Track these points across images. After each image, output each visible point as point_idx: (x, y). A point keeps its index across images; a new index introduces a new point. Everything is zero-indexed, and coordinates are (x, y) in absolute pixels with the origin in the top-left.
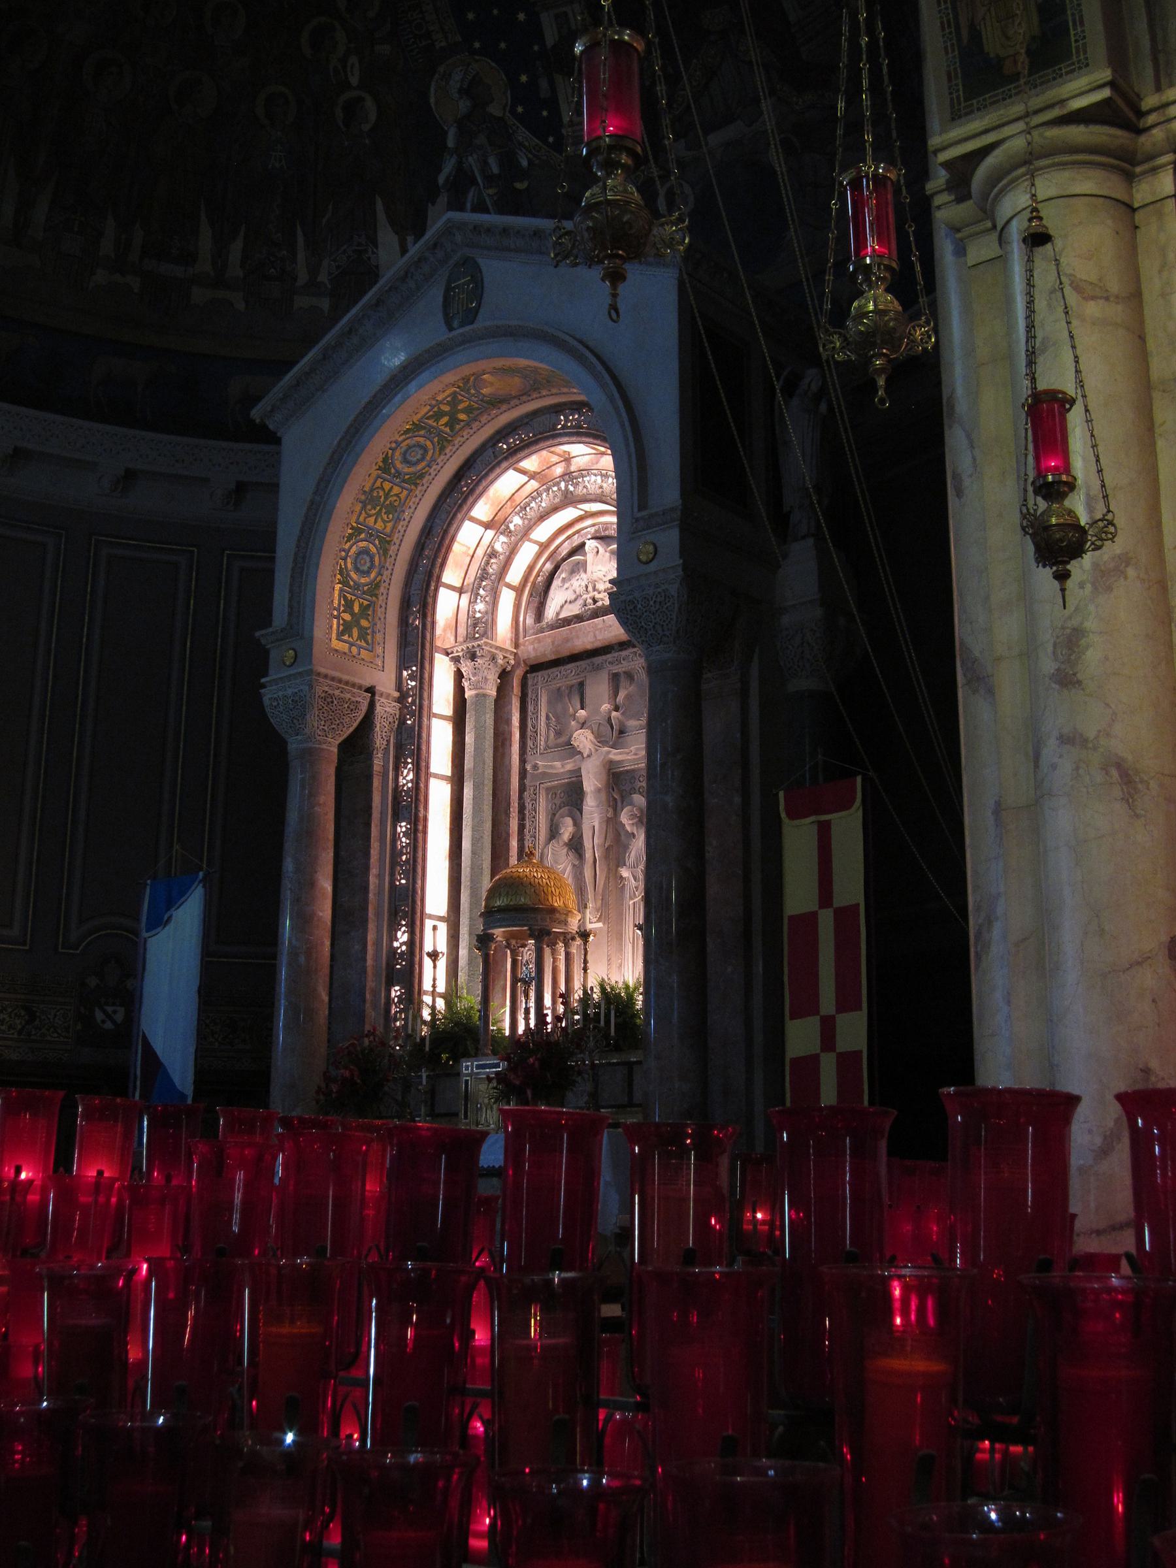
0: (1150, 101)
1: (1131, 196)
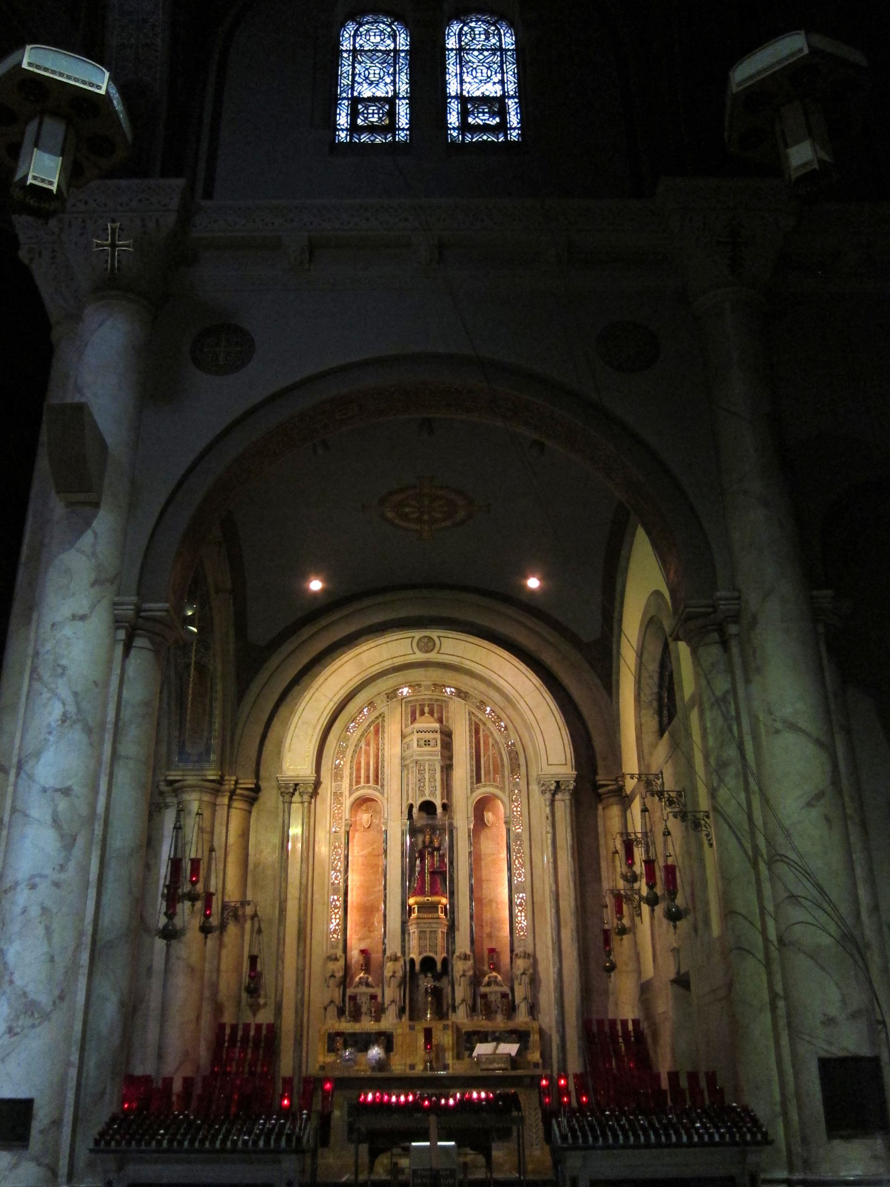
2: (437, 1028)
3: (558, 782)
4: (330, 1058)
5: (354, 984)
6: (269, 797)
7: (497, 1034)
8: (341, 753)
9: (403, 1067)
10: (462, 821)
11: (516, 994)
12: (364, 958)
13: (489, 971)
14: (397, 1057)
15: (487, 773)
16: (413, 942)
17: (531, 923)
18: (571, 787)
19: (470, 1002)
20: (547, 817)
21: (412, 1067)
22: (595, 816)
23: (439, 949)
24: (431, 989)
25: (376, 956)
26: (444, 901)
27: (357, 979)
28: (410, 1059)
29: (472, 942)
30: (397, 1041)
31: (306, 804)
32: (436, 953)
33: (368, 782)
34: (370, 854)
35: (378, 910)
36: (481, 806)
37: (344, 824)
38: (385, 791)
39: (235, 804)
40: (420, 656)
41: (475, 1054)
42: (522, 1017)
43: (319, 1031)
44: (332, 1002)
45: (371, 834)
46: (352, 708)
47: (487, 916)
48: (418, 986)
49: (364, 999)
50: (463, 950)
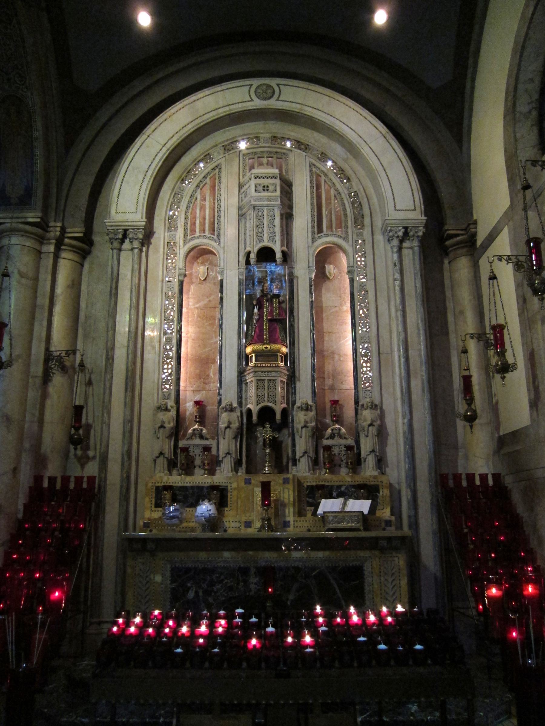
0: (52, 224)
1: (41, 249)
2: (276, 481)
3: (406, 228)
4: (157, 514)
5: (188, 436)
6: (102, 250)
7: (343, 489)
8: (175, 203)
9: (238, 525)
10: (303, 269)
11: (362, 446)
12: (199, 410)
13: (331, 423)
14: (231, 513)
15: (330, 227)
16: (251, 392)
17: (377, 374)
18: (420, 234)
19: (312, 454)
20: (395, 265)
21: (248, 524)
22: (441, 271)
23: (279, 398)
24: (270, 440)
25: (211, 408)
26: (284, 350)
27: (190, 431)
28: (244, 518)
29: (314, 392)
30: (232, 496)
31: (136, 251)
32: (275, 403)
33: (204, 231)
34: (206, 306)
35: (214, 362)
36: (323, 258)
37: (177, 274)
38: (222, 240)
39: (64, 254)
40: (258, 103)
41: (320, 511)
42: (369, 471)
43: (146, 485)
44: (161, 454)
45: (208, 286)
46: (186, 160)
47: (328, 368)
48: (256, 438)
49: (198, 451)
50: (304, 401)
